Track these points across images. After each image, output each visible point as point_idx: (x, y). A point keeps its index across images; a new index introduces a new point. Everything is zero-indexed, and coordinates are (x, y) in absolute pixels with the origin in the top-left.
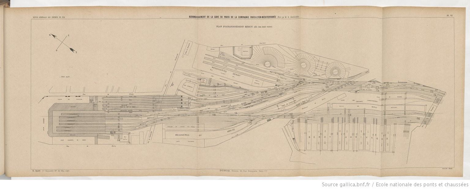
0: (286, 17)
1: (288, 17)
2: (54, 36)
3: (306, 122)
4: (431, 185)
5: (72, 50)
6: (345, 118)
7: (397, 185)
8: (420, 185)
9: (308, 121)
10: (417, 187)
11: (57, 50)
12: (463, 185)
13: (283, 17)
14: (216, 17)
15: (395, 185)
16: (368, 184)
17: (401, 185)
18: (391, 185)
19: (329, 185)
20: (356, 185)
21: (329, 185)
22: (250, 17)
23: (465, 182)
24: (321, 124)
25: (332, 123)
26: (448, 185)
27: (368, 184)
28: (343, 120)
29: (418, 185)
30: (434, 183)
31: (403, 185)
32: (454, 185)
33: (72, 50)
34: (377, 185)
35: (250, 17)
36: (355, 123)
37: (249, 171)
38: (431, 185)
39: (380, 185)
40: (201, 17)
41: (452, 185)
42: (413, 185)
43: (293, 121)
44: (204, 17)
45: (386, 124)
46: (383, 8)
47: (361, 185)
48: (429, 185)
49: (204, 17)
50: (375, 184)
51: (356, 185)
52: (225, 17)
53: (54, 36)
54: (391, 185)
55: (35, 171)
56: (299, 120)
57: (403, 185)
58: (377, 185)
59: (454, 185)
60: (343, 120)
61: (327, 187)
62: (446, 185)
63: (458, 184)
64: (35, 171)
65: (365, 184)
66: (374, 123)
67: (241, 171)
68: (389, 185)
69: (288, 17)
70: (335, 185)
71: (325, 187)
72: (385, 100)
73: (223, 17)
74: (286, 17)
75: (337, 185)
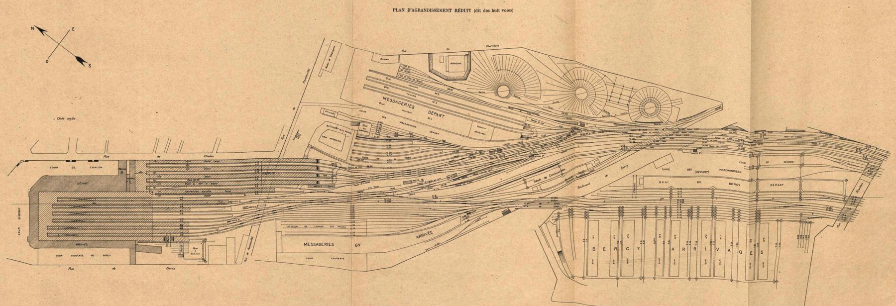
2: (41, 31)
3: (586, 216)
5: (80, 60)
28: (665, 213)
33: (80, 60)
43: (559, 214)
53: (41, 31)
56: (571, 212)
60: (665, 213)
66: (733, 219)
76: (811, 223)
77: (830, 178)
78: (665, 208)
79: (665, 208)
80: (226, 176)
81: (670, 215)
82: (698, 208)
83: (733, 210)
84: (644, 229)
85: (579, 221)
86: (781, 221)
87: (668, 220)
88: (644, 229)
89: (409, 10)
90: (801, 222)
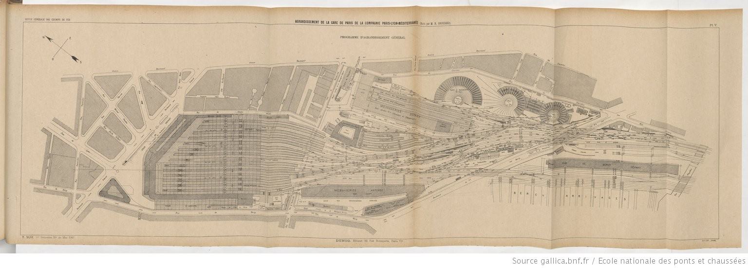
0: (432, 24)
1: (435, 23)
2: (49, 39)
3: (511, 181)
4: (686, 261)
5: (75, 58)
6: (609, 181)
7: (632, 261)
8: (668, 262)
9: (514, 180)
10: (663, 265)
11: (53, 59)
12: (738, 261)
13: (428, 24)
14: (334, 23)
15: (629, 262)
16: (585, 261)
17: (637, 261)
18: (623, 261)
19: (524, 262)
20: (566, 261)
21: (524, 262)
22: (381, 23)
23: (740, 256)
24: (531, 186)
25: (622, 190)
26: (714, 261)
27: (585, 261)
28: (605, 184)
29: (665, 261)
30: (691, 259)
31: (642, 261)
32: (723, 262)
33: (75, 58)
34: (601, 262)
35: (381, 23)
36: (578, 186)
37: (377, 241)
38: (686, 261)
39: (605, 261)
40: (313, 21)
41: (719, 262)
42: (657, 262)
43: (492, 180)
44: (316, 22)
45: (623, 189)
46: (556, 11)
47: (575, 261)
48: (682, 261)
49: (316, 22)
50: (597, 260)
51: (566, 261)
52: (347, 23)
53: (49, 39)
54: (623, 261)
55: (25, 237)
56: (500, 180)
57: (642, 261)
58: (601, 262)
59: (723, 262)
60: (605, 184)
61: (521, 265)
62: (710, 261)
63: (729, 261)
64: (25, 237)
65: (582, 261)
66: (605, 188)
67: (366, 241)
68: (619, 261)
69: (435, 23)
70: (532, 261)
71: (517, 265)
72: (622, 155)
73: (344, 23)
74: (432, 24)
75: (536, 261)
76: (657, 192)
77: (368, 211)
78: (562, 179)
79: (562, 179)
80: (282, 153)
81: (565, 184)
82: (583, 180)
83: (605, 181)
84: (669, 156)
85: (506, 185)
86: (637, 190)
87: (563, 188)
88: (669, 156)
89: (361, 37)
90: (650, 192)
